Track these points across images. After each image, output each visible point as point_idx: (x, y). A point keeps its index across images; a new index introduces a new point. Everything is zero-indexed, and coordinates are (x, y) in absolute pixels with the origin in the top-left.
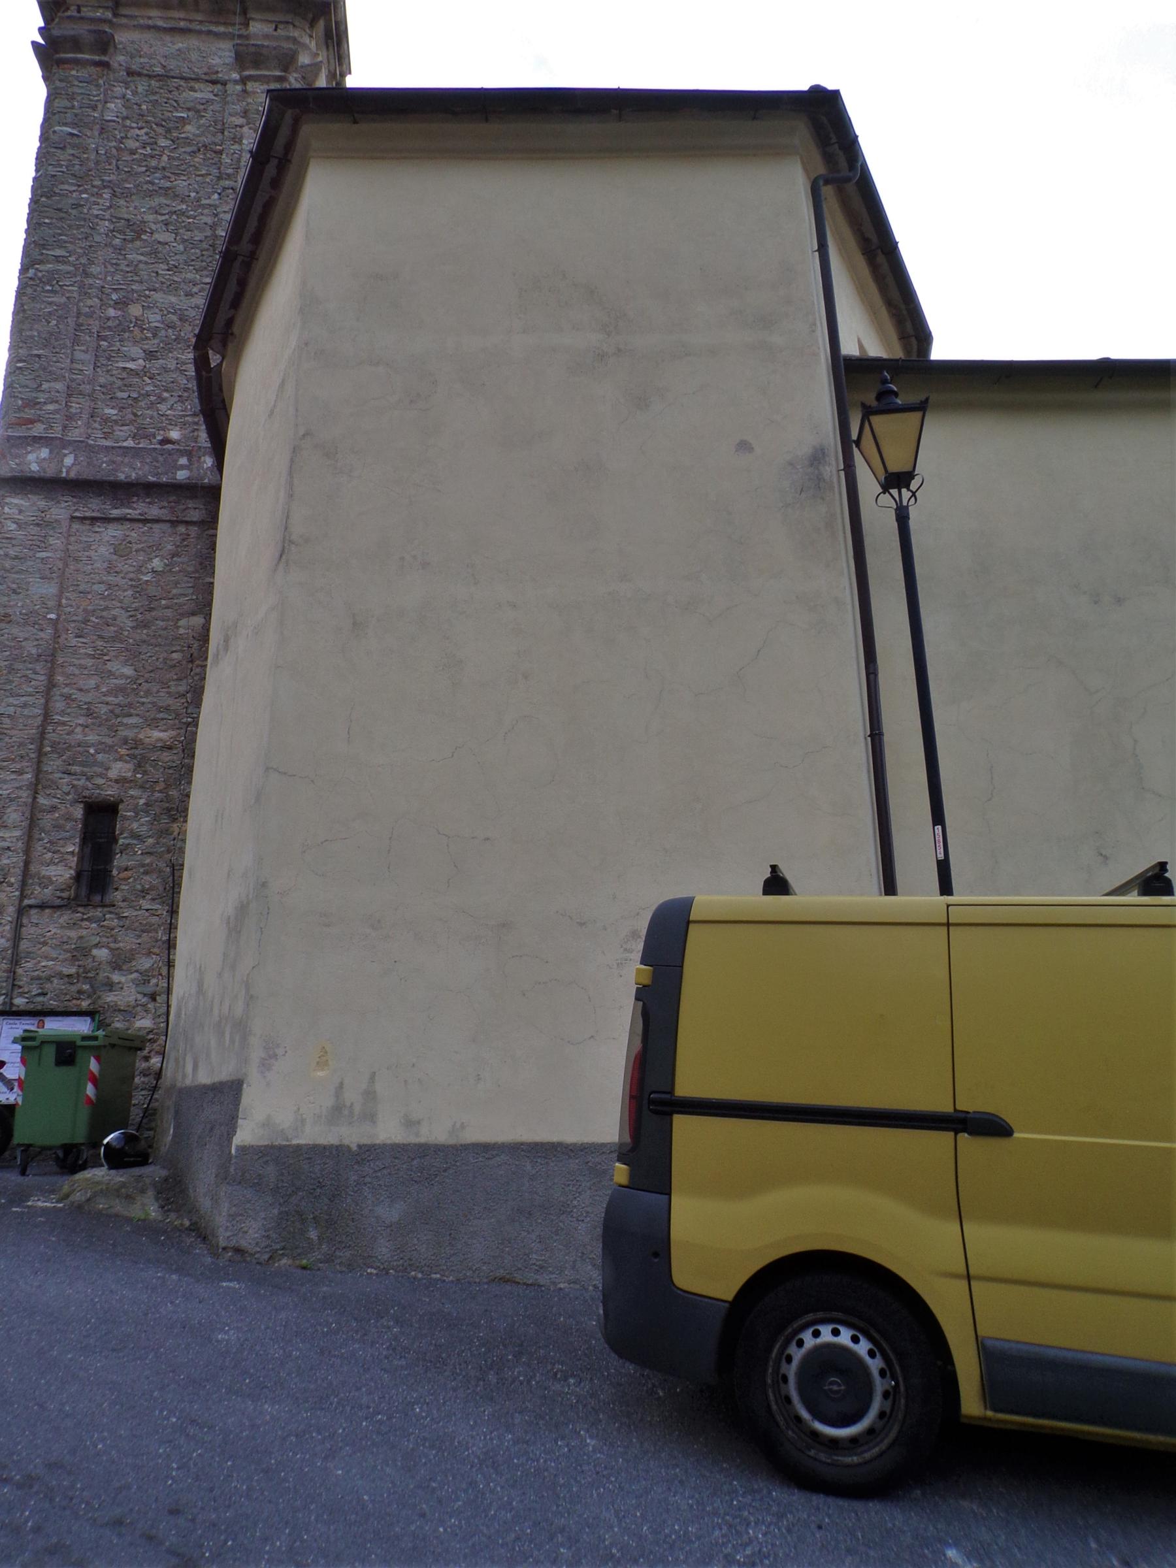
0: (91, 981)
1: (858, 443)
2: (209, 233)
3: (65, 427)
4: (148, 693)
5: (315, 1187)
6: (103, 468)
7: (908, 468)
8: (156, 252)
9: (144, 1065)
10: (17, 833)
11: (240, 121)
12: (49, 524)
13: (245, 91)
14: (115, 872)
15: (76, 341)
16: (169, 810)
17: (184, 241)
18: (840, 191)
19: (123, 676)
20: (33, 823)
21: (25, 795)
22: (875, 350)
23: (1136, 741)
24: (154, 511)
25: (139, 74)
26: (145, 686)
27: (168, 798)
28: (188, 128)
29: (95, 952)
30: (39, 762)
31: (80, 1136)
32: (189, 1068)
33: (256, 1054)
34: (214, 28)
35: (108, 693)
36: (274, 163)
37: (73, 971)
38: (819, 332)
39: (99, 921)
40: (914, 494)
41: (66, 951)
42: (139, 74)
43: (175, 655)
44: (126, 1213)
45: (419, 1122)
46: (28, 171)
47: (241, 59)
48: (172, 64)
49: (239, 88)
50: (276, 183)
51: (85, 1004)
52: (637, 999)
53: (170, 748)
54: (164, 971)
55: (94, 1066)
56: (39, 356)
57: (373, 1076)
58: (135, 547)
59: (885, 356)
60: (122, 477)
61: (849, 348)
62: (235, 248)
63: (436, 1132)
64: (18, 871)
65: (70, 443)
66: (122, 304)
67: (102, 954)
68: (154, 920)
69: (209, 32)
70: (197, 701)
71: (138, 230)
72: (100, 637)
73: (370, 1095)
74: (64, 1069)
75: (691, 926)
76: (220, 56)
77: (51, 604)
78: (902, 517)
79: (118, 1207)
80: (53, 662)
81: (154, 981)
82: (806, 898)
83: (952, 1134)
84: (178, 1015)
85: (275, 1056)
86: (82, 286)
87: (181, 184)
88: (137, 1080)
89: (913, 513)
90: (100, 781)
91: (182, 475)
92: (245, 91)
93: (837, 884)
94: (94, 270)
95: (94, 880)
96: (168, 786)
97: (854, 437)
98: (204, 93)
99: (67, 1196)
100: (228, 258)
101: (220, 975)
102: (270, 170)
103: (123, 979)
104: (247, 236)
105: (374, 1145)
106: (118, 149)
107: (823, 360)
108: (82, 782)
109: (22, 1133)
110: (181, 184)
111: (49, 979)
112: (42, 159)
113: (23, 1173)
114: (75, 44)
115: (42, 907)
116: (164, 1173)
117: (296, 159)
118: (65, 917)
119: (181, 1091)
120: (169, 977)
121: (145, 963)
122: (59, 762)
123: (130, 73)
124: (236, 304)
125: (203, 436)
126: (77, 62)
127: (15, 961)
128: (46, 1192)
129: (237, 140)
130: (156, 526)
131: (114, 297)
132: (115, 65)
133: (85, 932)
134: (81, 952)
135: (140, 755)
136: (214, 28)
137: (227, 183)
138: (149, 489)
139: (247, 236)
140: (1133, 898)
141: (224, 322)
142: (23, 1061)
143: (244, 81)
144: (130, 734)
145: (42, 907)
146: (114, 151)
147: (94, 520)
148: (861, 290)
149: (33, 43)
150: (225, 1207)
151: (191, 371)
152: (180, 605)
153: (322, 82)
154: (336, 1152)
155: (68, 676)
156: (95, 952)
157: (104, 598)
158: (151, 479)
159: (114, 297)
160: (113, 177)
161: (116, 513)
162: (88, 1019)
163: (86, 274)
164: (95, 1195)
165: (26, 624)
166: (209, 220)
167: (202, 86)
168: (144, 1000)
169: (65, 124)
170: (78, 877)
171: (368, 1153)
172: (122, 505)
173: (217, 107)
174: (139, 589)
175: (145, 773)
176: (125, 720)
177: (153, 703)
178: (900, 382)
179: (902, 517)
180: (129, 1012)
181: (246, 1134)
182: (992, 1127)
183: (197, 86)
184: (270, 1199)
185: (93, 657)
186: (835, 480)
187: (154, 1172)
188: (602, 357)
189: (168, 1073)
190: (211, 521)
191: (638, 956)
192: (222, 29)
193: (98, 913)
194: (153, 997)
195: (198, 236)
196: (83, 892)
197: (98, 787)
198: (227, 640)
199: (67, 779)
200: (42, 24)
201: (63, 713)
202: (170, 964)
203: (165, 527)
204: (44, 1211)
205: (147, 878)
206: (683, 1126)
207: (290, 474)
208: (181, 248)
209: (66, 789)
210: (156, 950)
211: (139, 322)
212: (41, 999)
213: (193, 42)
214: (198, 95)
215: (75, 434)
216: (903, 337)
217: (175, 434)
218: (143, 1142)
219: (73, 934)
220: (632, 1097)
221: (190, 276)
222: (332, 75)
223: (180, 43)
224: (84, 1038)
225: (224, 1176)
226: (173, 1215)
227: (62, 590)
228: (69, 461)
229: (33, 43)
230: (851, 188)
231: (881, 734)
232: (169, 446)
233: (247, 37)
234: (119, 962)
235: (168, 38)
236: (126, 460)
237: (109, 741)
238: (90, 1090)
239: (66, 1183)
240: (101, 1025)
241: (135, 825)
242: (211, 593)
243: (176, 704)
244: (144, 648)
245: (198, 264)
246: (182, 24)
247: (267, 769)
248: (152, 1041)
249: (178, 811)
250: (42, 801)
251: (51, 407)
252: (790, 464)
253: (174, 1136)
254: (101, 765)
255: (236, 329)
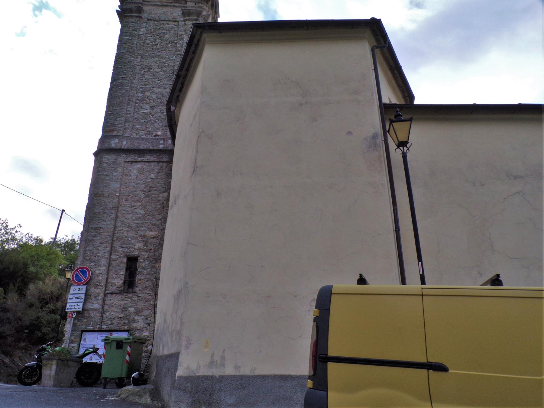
0: (128, 319)
1: (388, 132)
2: (172, 68)
3: (124, 132)
4: (149, 219)
5: (204, 392)
6: (136, 145)
7: (406, 140)
8: (155, 75)
9: (146, 349)
10: (104, 268)
11: (183, 33)
12: (117, 164)
13: (185, 24)
14: (136, 281)
15: (128, 104)
16: (155, 259)
17: (164, 71)
18: (382, 51)
19: (140, 213)
20: (110, 264)
21: (107, 255)
22: (394, 101)
23: (490, 234)
24: (152, 159)
25: (151, 20)
26: (148, 217)
27: (155, 255)
28: (166, 36)
29: (129, 309)
30: (112, 244)
31: (124, 375)
32: (161, 349)
33: (184, 343)
34: (175, 4)
35: (136, 219)
36: (194, 46)
37: (122, 316)
38: (375, 95)
39: (131, 298)
40: (408, 149)
41: (120, 309)
42: (151, 20)
43: (158, 206)
44: (139, 402)
45: (240, 367)
46: (114, 51)
47: (184, 14)
48: (162, 16)
49: (183, 23)
50: (194, 52)
51: (126, 328)
52: (314, 321)
53: (156, 238)
54: (153, 316)
55: (129, 349)
56: (116, 110)
57: (224, 352)
58: (145, 170)
59: (398, 103)
60: (141, 147)
61: (385, 100)
62: (180, 73)
63: (246, 371)
64: (104, 281)
65: (125, 137)
66: (143, 92)
67: (132, 310)
68: (150, 297)
69: (174, 6)
70: (165, 222)
71: (149, 69)
72: (133, 201)
73: (223, 358)
74: (120, 351)
75: (332, 295)
76: (177, 13)
77: (117, 190)
78: (404, 156)
79: (137, 400)
80: (118, 210)
81: (149, 319)
82: (372, 286)
83: (426, 370)
84: (158, 330)
85: (190, 344)
86: (131, 87)
87: (164, 54)
88: (143, 354)
89: (408, 155)
90: (132, 250)
91: (161, 147)
92: (185, 24)
93: (384, 280)
94: (135, 81)
95: (130, 283)
96: (155, 251)
97: (387, 130)
98: (172, 25)
99: (119, 396)
100: (178, 76)
101: (172, 316)
102: (193, 48)
103: (139, 318)
104: (185, 69)
105: (224, 376)
106: (144, 43)
107: (376, 104)
108: (126, 250)
109: (105, 373)
110: (164, 54)
111: (114, 319)
112: (119, 47)
113: (104, 388)
114: (131, 11)
115: (112, 293)
116: (153, 387)
117: (201, 44)
118: (120, 297)
119: (158, 357)
120: (155, 317)
121: (146, 313)
122: (119, 243)
123: (148, 20)
124: (180, 90)
125: (168, 133)
126: (131, 16)
127: (103, 313)
128: (112, 394)
129: (182, 39)
130: (152, 163)
131: (141, 90)
132: (143, 17)
133: (126, 302)
134: (125, 309)
135: (145, 240)
136: (175, 4)
137: (178, 53)
138: (150, 151)
139: (185, 69)
140: (489, 287)
141: (177, 95)
142: (105, 348)
143: (185, 21)
144: (142, 233)
145: (112, 293)
146: (142, 44)
147: (132, 162)
148: (389, 82)
149: (117, 11)
150: (173, 398)
151: (165, 112)
152: (160, 189)
153: (210, 20)
154: (212, 378)
155: (122, 214)
156: (129, 309)
157: (135, 188)
158: (151, 148)
159: (141, 90)
160: (142, 52)
161: (139, 159)
162: (127, 333)
163: (132, 83)
164: (129, 395)
165: (109, 197)
166: (172, 64)
167: (171, 23)
168: (146, 325)
169: (127, 36)
170: (125, 282)
171: (222, 378)
172: (141, 157)
173: (176, 29)
174: (146, 184)
175: (147, 246)
176: (141, 229)
177: (151, 223)
178: (403, 111)
179: (404, 156)
180: (141, 330)
181: (180, 372)
182: (441, 368)
183: (169, 23)
184: (188, 395)
185: (131, 207)
186: (381, 144)
187: (149, 387)
188: (301, 105)
189: (154, 351)
190: (170, 161)
191: (314, 307)
192: (178, 5)
193: (131, 295)
194: (149, 325)
195: (168, 69)
196: (126, 288)
197: (131, 251)
198: (175, 201)
199: (121, 249)
200: (120, 4)
201: (120, 227)
202: (155, 313)
203: (156, 164)
204: (112, 401)
205: (148, 283)
206: (331, 366)
207: (197, 145)
208: (163, 73)
209: (121, 252)
210: (150, 308)
211: (149, 98)
212: (111, 326)
213: (169, 9)
214: (170, 26)
215: (127, 134)
216: (404, 97)
217: (159, 133)
218: (145, 377)
219: (122, 303)
220: (313, 356)
221: (166, 82)
222: (213, 18)
223: (165, 9)
224: (126, 339)
225: (173, 387)
226: (155, 402)
227: (121, 185)
228: (125, 143)
229: (117, 11)
230: (385, 49)
231: (399, 230)
232: (157, 137)
233: (186, 7)
234: (138, 312)
235: (160, 8)
236: (143, 142)
237: (136, 236)
238: (127, 358)
239: (119, 391)
240: (131, 335)
241: (143, 265)
242: (170, 185)
243: (158, 223)
244: (148, 204)
245: (168, 78)
246: (165, 4)
247: (188, 243)
248: (149, 340)
249: (158, 259)
250: (113, 257)
251: (119, 126)
252: (365, 139)
253: (156, 373)
254: (133, 244)
255: (180, 98)
